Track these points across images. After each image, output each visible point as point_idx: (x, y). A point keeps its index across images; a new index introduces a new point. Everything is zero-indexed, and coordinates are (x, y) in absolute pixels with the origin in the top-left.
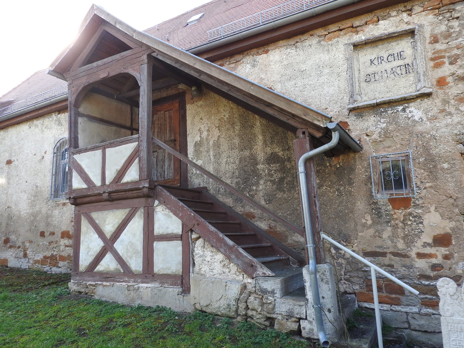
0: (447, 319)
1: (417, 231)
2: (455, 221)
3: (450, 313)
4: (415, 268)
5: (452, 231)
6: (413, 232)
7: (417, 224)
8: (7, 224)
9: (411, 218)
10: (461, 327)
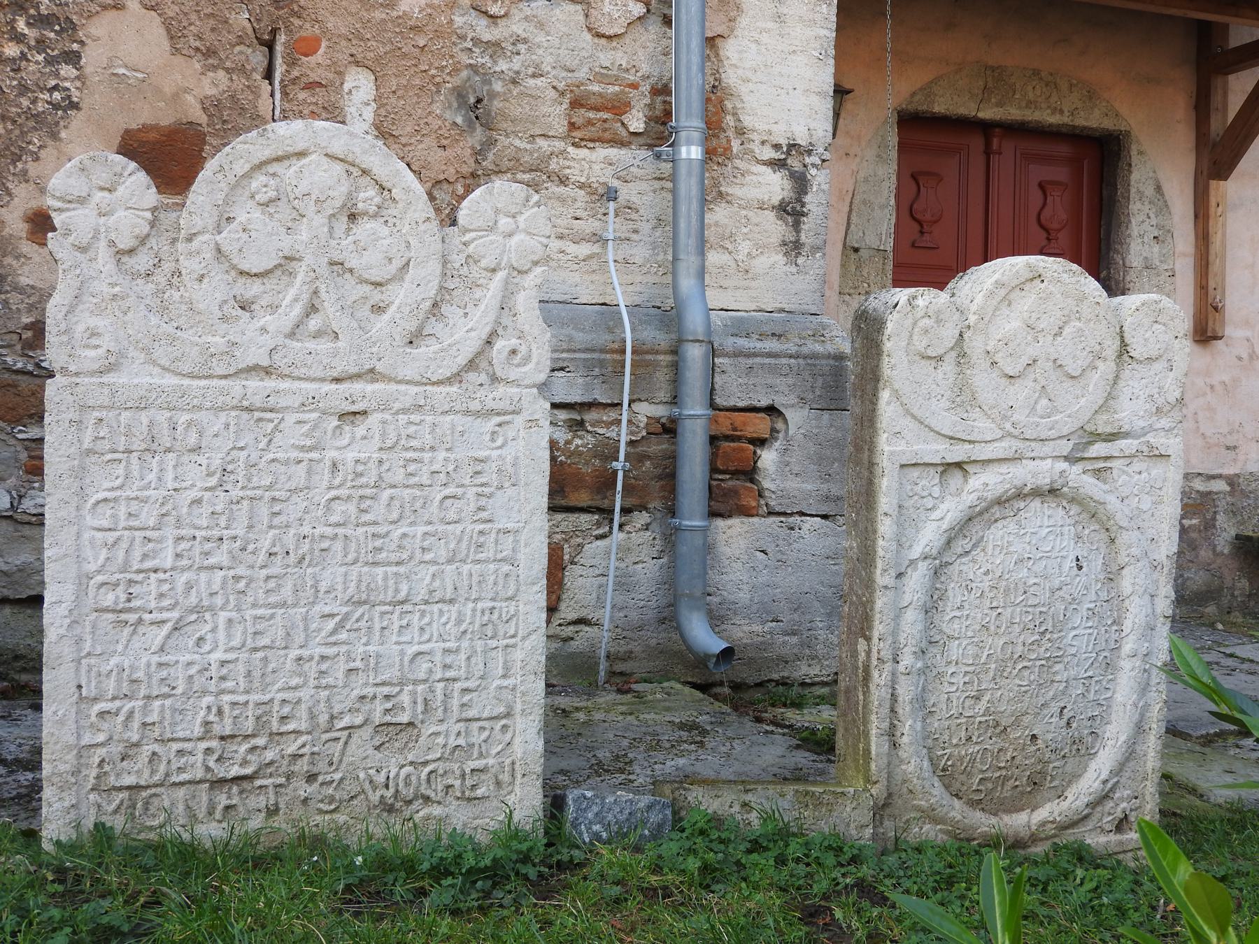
0: (79, 389)
1: (46, 96)
2: (227, 70)
3: (101, 351)
4: (17, 288)
5: (210, 116)
6: (25, 102)
7: (50, 61)
9: (21, 25)
10: (151, 424)
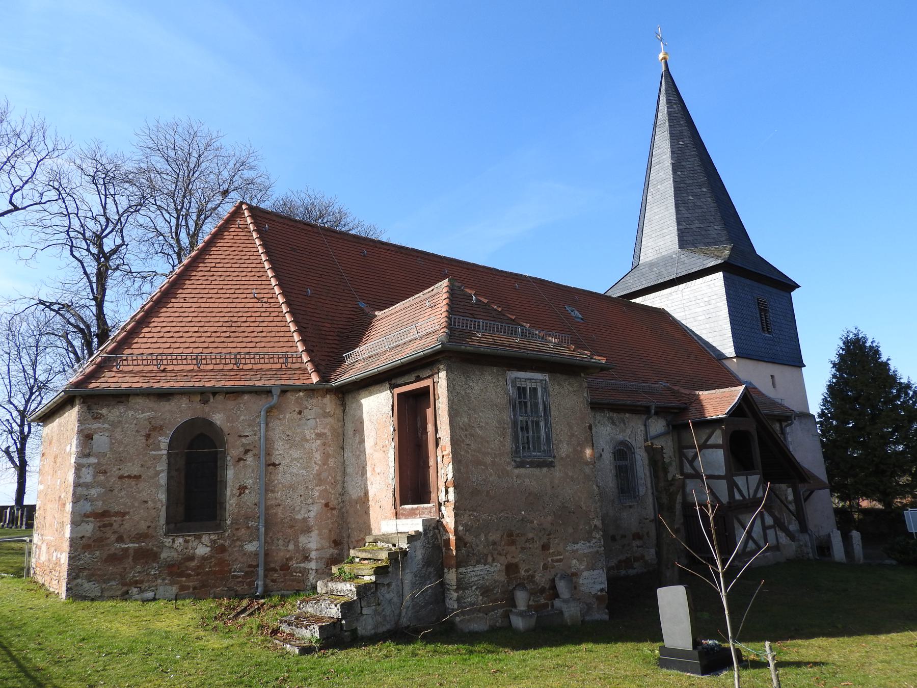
8: (266, 555)
